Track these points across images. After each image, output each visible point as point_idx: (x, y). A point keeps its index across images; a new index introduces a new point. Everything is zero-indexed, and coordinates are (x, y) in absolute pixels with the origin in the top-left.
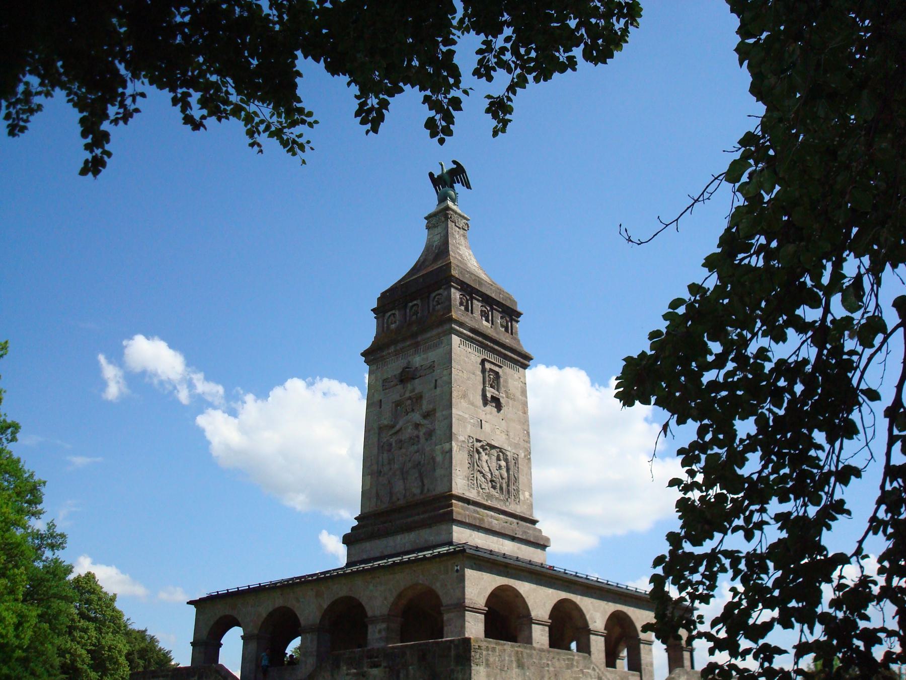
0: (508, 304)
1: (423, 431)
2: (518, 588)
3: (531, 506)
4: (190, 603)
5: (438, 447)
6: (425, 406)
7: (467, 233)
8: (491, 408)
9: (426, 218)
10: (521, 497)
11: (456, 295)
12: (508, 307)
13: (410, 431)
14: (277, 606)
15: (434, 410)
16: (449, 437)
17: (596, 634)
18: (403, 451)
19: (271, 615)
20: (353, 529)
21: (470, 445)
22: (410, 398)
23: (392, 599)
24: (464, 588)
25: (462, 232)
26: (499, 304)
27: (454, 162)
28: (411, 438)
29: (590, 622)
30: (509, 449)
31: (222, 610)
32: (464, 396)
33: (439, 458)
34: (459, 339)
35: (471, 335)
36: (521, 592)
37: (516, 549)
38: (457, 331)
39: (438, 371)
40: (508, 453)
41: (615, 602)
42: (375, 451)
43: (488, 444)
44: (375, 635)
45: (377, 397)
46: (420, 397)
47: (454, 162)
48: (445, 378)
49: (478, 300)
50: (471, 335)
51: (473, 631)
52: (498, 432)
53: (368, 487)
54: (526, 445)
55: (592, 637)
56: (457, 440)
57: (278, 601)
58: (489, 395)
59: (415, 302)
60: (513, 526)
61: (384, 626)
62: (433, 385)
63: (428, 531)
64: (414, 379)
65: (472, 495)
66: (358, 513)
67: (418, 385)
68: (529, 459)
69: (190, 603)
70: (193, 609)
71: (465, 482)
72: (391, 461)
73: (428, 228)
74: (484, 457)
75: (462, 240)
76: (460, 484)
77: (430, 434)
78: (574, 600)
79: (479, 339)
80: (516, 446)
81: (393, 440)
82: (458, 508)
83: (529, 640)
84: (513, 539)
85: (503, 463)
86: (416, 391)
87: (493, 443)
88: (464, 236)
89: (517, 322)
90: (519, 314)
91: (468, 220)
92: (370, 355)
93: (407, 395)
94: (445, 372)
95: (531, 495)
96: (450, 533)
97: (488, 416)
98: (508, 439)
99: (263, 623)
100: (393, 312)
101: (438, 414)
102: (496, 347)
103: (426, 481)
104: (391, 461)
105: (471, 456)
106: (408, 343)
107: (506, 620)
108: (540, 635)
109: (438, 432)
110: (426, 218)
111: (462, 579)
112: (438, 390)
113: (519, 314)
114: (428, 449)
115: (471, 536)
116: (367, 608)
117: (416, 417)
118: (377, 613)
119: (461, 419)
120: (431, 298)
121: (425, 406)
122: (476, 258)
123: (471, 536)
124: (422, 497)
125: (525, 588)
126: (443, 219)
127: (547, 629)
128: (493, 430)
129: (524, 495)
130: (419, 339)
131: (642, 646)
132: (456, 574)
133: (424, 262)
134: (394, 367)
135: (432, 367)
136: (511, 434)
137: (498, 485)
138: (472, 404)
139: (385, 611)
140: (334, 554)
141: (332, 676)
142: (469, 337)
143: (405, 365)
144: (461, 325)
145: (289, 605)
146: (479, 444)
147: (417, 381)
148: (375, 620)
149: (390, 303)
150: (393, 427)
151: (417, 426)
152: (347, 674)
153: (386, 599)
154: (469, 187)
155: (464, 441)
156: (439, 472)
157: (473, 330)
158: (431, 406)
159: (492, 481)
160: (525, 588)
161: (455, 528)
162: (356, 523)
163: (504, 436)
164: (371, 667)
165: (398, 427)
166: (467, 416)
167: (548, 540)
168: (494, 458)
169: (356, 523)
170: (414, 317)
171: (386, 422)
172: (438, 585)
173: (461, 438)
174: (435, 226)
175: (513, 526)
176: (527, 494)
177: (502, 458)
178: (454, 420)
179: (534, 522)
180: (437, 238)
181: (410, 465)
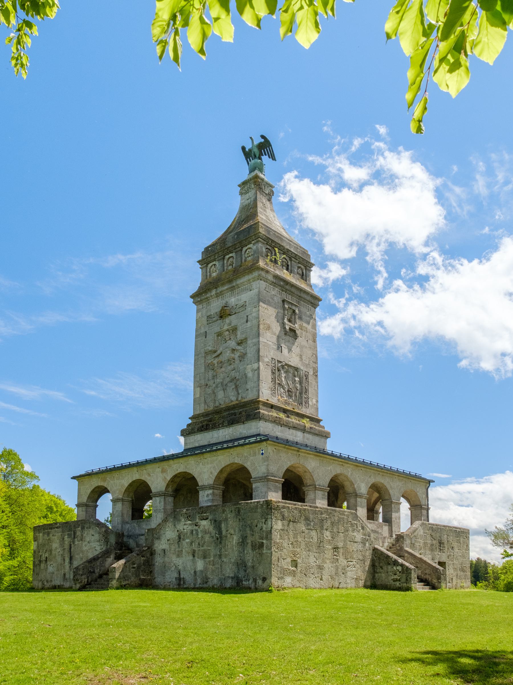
1: (237, 354)
4: (74, 478)
5: (250, 366)
6: (240, 336)
9: (239, 186)
10: (310, 403)
13: (228, 354)
14: (134, 479)
15: (246, 339)
18: (223, 369)
19: (130, 485)
20: (189, 425)
22: (228, 330)
23: (216, 474)
27: (263, 137)
28: (229, 360)
31: (96, 482)
33: (250, 375)
39: (248, 309)
42: (203, 370)
43: (286, 364)
44: (205, 498)
45: (203, 330)
46: (234, 330)
47: (263, 137)
48: (254, 315)
53: (198, 396)
57: (135, 475)
58: (287, 328)
59: (231, 255)
61: (210, 491)
62: (245, 320)
63: (242, 426)
65: (274, 401)
67: (233, 320)
69: (74, 478)
70: (76, 482)
71: (269, 392)
72: (214, 377)
73: (241, 194)
80: (307, 366)
81: (215, 362)
86: (233, 325)
87: (290, 363)
92: (199, 297)
93: (226, 327)
94: (254, 310)
99: (125, 490)
100: (214, 263)
101: (249, 342)
103: (240, 391)
104: (214, 377)
106: (226, 288)
109: (249, 355)
110: (239, 186)
112: (249, 323)
114: (241, 368)
116: (198, 480)
118: (206, 483)
120: (243, 253)
124: (237, 402)
130: (234, 284)
132: (261, 456)
134: (215, 306)
136: (304, 358)
139: (211, 482)
141: (175, 525)
143: (224, 305)
145: (143, 478)
148: (204, 488)
149: (211, 255)
150: (215, 352)
151: (233, 350)
152: (185, 525)
153: (211, 473)
154: (274, 159)
155: (268, 362)
156: (250, 385)
158: (244, 336)
159: (288, 391)
162: (190, 421)
164: (201, 520)
165: (219, 352)
171: (210, 348)
172: (249, 463)
173: (266, 360)
174: (246, 193)
181: (228, 379)
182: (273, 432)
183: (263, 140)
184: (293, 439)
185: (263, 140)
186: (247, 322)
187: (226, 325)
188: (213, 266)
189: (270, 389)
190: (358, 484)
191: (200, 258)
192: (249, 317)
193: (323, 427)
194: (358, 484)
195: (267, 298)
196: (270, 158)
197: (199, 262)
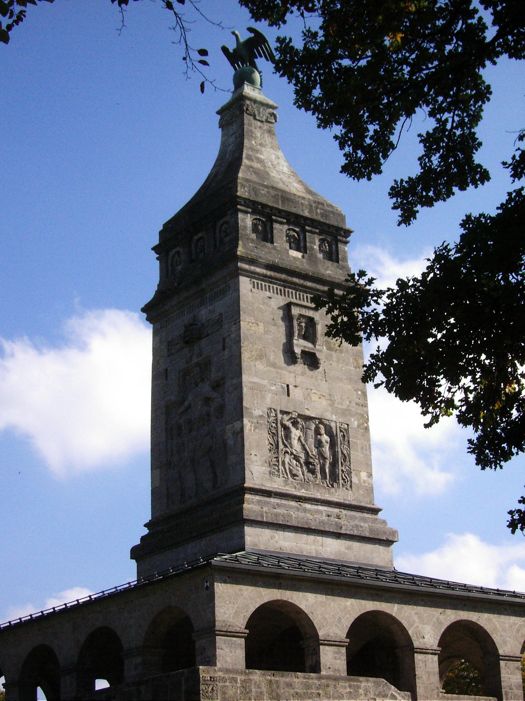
0: (332, 221)
2: (297, 603)
3: (370, 490)
5: (229, 427)
6: (214, 375)
7: (276, 127)
8: (300, 367)
9: (218, 113)
10: (355, 480)
11: (246, 221)
12: (329, 226)
15: (223, 378)
16: (239, 413)
17: (424, 651)
20: (143, 539)
21: (272, 419)
22: (198, 364)
24: (214, 608)
25: (266, 126)
26: (313, 223)
29: (414, 638)
30: (334, 418)
32: (261, 357)
33: (231, 442)
34: (248, 279)
35: (269, 273)
36: (302, 607)
37: (343, 549)
38: (246, 271)
40: (333, 425)
41: (455, 607)
43: (300, 416)
49: (281, 223)
50: (269, 273)
51: (228, 659)
52: (315, 398)
54: (360, 410)
55: (418, 657)
56: (251, 416)
58: (298, 350)
59: (200, 235)
60: (350, 521)
61: (139, 660)
62: (221, 346)
64: (200, 338)
65: (277, 484)
66: (147, 517)
68: (367, 429)
71: (266, 469)
74: (296, 433)
75: (267, 139)
76: (257, 470)
77: (221, 409)
78: (388, 611)
79: (281, 276)
80: (345, 412)
82: (251, 505)
83: (316, 668)
84: (338, 536)
85: (325, 438)
87: (307, 413)
88: (270, 132)
89: (346, 243)
90: (348, 233)
91: (274, 108)
93: (195, 360)
95: (370, 475)
96: (242, 537)
97: (299, 379)
98: (332, 405)
102: (309, 284)
105: (274, 435)
107: (280, 643)
108: (333, 659)
110: (218, 113)
111: (210, 598)
112: (226, 352)
113: (348, 233)
115: (272, 537)
117: (206, 388)
119: (258, 388)
121: (214, 375)
122: (287, 161)
123: (272, 537)
125: (307, 601)
126: (238, 113)
127: (344, 650)
128: (307, 396)
129: (359, 477)
131: (502, 663)
133: (215, 176)
135: (219, 322)
137: (318, 468)
138: (274, 365)
140: (126, 574)
142: (266, 276)
144: (252, 262)
146: (286, 417)
147: (204, 342)
150: (182, 403)
151: (207, 401)
155: (261, 416)
156: (233, 458)
157: (270, 267)
158: (220, 374)
160: (307, 601)
161: (248, 530)
162: (146, 531)
163: (324, 403)
165: (186, 404)
166: (265, 382)
167: (394, 533)
168: (311, 433)
169: (146, 531)
170: (202, 255)
173: (257, 412)
175: (350, 521)
176: (363, 475)
177: (323, 431)
178: (245, 390)
179: (375, 511)
180: (232, 140)
182: (272, 541)
183: (252, 35)
184: (317, 551)
185: (252, 35)
186: (224, 349)
187: (195, 357)
188: (177, 256)
189: (267, 465)
190: (417, 627)
191: (157, 242)
192: (227, 340)
193: (384, 522)
194: (417, 627)
195: (256, 305)
196: (267, 60)
197: (341, 172)
